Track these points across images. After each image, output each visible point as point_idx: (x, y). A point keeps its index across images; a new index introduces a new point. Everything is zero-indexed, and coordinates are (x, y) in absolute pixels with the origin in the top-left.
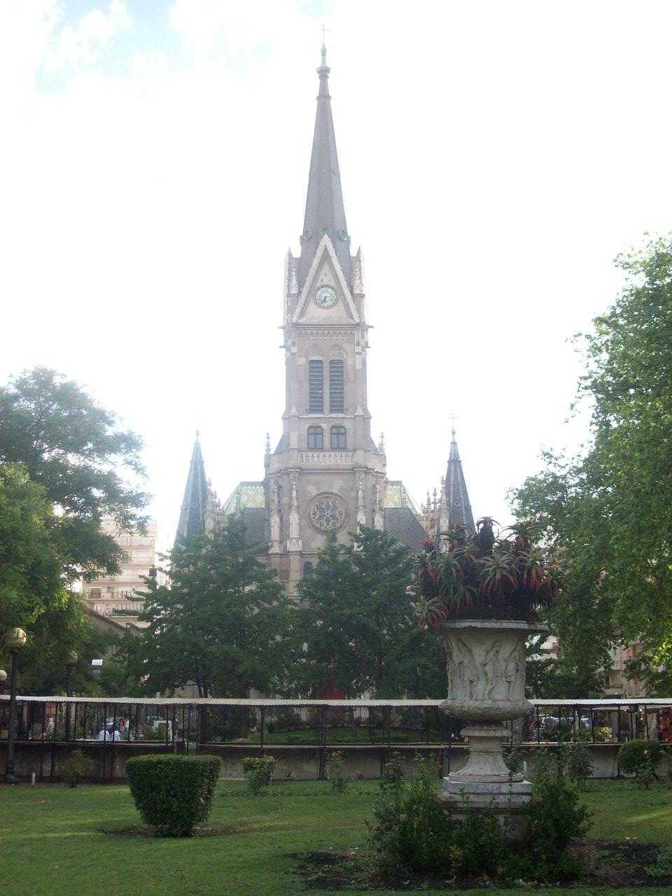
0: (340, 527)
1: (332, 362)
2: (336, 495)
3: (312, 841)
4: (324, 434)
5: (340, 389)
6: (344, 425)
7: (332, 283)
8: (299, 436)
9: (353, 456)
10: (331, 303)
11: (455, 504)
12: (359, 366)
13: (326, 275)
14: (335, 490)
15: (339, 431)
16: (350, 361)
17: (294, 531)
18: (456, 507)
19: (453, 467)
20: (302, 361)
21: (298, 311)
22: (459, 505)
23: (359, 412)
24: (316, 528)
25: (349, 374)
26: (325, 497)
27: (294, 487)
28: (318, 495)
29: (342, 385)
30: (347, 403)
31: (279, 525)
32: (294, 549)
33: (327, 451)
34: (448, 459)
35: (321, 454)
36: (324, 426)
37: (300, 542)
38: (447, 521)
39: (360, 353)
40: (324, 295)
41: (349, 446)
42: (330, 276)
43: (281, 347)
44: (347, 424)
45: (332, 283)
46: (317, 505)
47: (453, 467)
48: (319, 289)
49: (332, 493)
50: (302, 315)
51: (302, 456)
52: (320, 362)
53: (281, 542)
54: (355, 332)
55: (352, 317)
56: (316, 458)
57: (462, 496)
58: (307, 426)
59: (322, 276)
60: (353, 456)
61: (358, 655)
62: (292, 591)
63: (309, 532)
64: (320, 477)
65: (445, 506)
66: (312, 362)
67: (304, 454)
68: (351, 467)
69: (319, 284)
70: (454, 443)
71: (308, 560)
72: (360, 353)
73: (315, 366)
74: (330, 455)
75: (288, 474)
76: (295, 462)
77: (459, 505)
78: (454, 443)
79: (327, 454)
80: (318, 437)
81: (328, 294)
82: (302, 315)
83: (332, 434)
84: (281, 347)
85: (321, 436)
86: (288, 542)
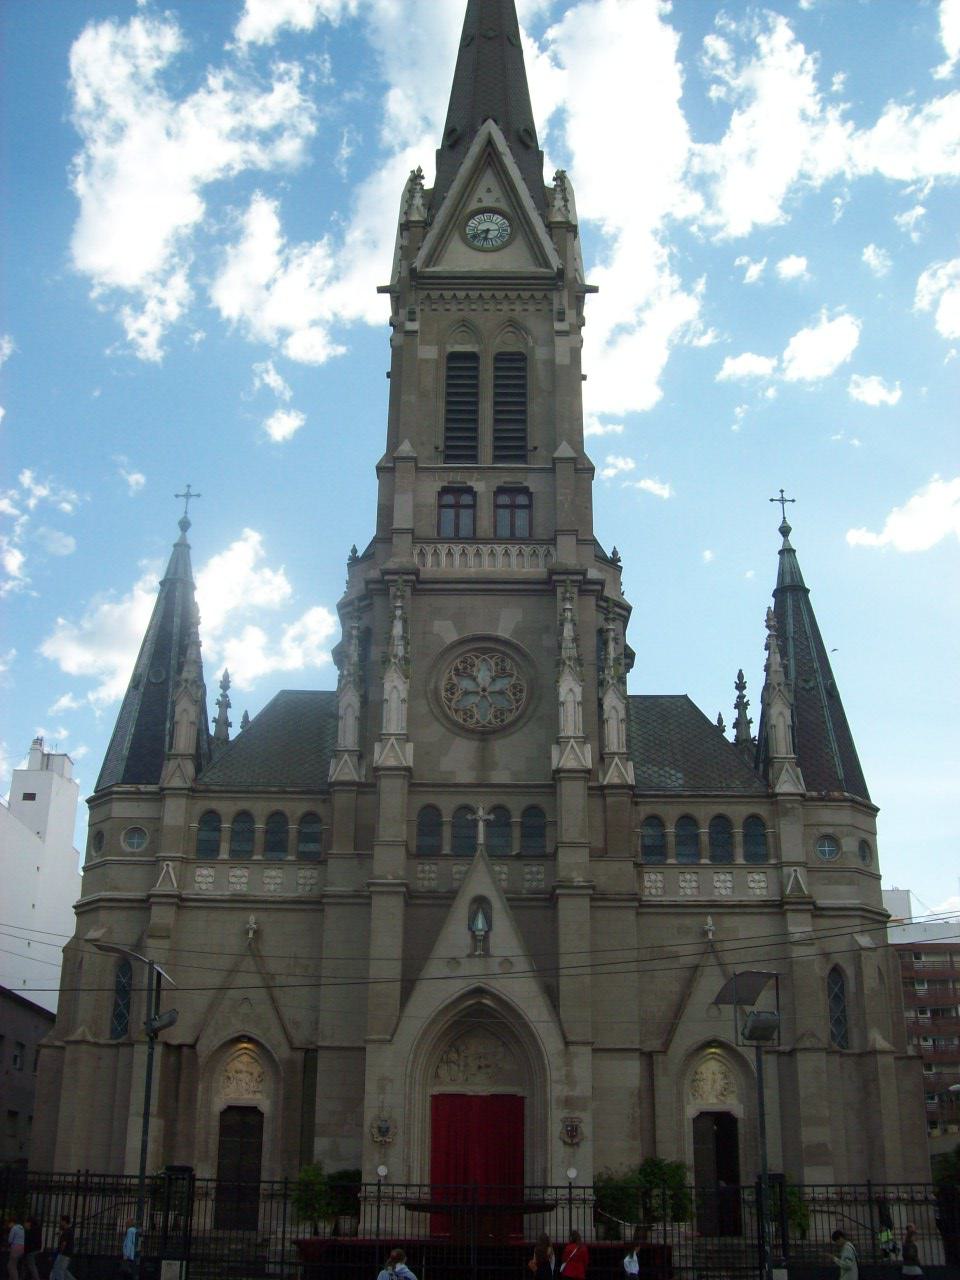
0: (513, 723)
1: (500, 357)
2: (506, 643)
3: (422, 444)
4: (478, 507)
5: (517, 421)
6: (525, 484)
7: (503, 205)
8: (417, 507)
9: (548, 554)
10: (496, 216)
11: (801, 684)
12: (562, 358)
13: (489, 190)
14: (504, 632)
15: (513, 496)
16: (540, 354)
17: (394, 719)
18: (803, 688)
19: (789, 602)
20: (429, 352)
21: (423, 253)
22: (811, 684)
23: (564, 450)
24: (455, 724)
25: (538, 376)
26: (476, 650)
27: (398, 613)
28: (462, 642)
29: (524, 404)
30: (536, 435)
31: (357, 714)
32: (392, 763)
33: (486, 541)
34: (774, 586)
35: (471, 550)
36: (479, 486)
37: (410, 747)
38: (788, 713)
39: (565, 333)
40: (483, 227)
41: (540, 532)
42: (497, 192)
43: (381, 290)
44: (533, 482)
45: (503, 205)
46: (457, 669)
47: (789, 602)
48: (473, 215)
49: (497, 640)
50: (431, 259)
51: (422, 554)
52: (473, 357)
53: (361, 757)
54: (555, 296)
55: (547, 264)
56: (457, 557)
57: (816, 665)
58: (438, 486)
59: (481, 192)
60: (548, 554)
61: (230, 1250)
62: (326, 238)
63: (435, 731)
64: (467, 601)
65: (781, 678)
66: (453, 357)
67: (429, 549)
68: (544, 576)
69: (474, 205)
70: (787, 552)
71: (431, 799)
72: (565, 333)
73: (461, 367)
74: (492, 554)
75: (385, 592)
76: (404, 560)
77: (811, 684)
78: (787, 552)
79: (485, 549)
80: (465, 514)
81: (494, 225)
82: (431, 259)
83: (497, 506)
84: (381, 290)
85: (471, 511)
86: (377, 747)
